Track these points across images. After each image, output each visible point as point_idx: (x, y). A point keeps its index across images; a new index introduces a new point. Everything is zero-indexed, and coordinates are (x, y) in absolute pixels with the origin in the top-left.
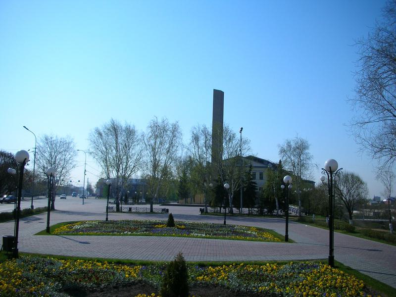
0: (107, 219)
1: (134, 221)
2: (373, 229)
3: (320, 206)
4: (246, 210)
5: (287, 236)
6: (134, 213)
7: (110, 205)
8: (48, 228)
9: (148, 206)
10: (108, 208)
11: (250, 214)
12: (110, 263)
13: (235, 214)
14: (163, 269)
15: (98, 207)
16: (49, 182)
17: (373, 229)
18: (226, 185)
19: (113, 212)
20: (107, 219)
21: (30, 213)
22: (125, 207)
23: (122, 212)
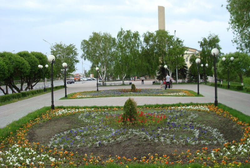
0: (98, 90)
1: (103, 91)
2: (199, 76)
3: (237, 8)
4: (180, 81)
5: (198, 93)
6: (113, 86)
7: (99, 83)
8: (66, 96)
9: (122, 82)
10: (97, 84)
11: (183, 83)
12: (101, 108)
13: (208, 82)
14: (130, 110)
15: (92, 84)
16: (8, 69)
17: (199, 76)
18: (166, 66)
19: (101, 86)
20: (98, 90)
21: (57, 88)
22: (108, 83)
23: (106, 86)
